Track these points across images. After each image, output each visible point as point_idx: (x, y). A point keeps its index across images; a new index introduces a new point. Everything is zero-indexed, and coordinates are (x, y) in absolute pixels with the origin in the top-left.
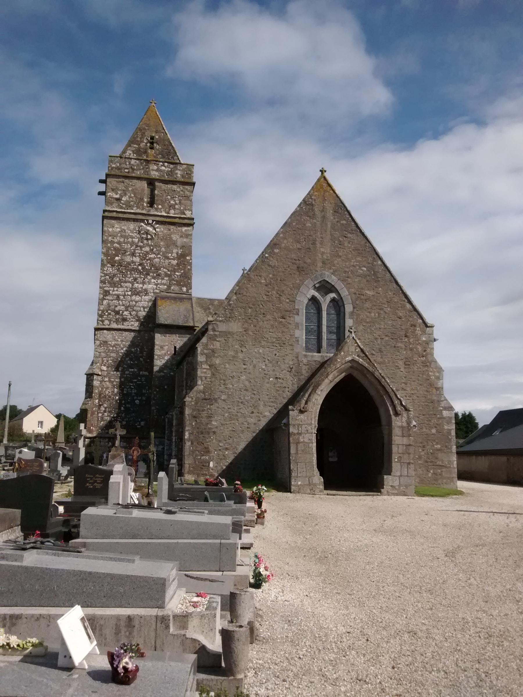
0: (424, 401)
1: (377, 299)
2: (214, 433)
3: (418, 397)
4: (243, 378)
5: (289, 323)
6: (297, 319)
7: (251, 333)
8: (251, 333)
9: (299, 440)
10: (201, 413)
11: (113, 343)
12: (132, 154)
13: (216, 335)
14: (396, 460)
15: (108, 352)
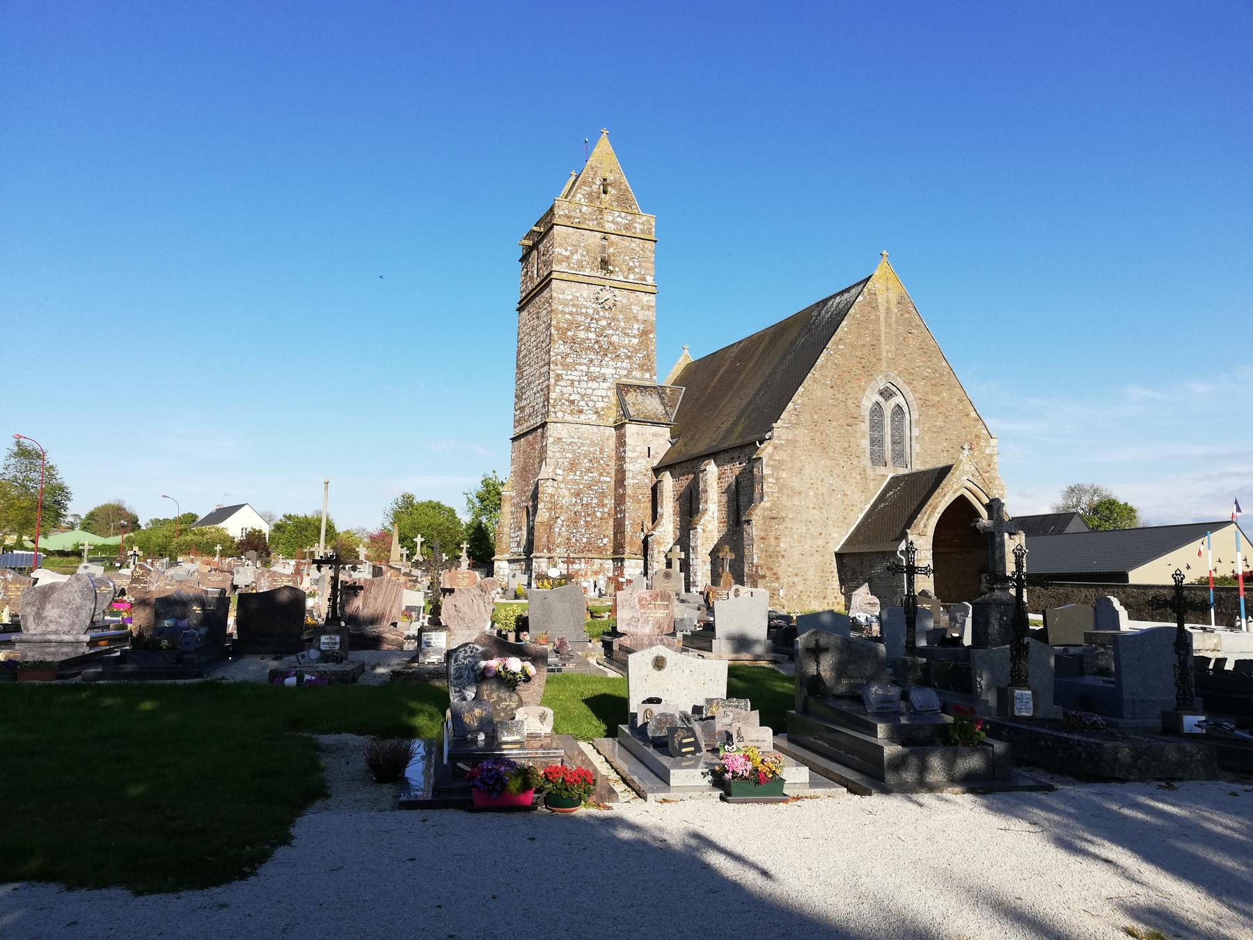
2: (783, 556)
8: (818, 442)
13: (782, 445)
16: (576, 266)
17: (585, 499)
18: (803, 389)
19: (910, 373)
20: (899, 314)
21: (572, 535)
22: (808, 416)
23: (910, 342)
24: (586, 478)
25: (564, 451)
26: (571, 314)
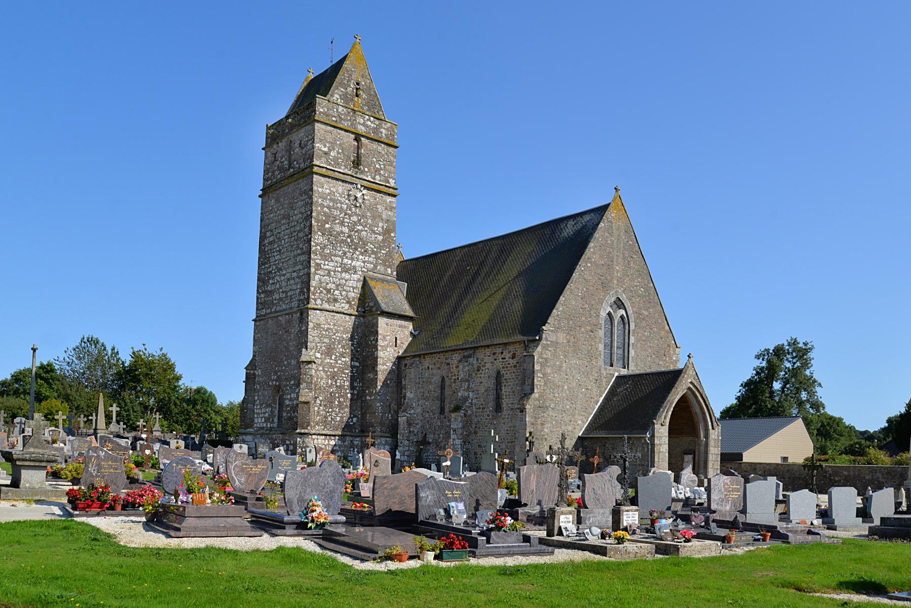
2: (546, 439)
17: (338, 381)
18: (564, 299)
19: (631, 291)
24: (339, 362)
26: (328, 207)
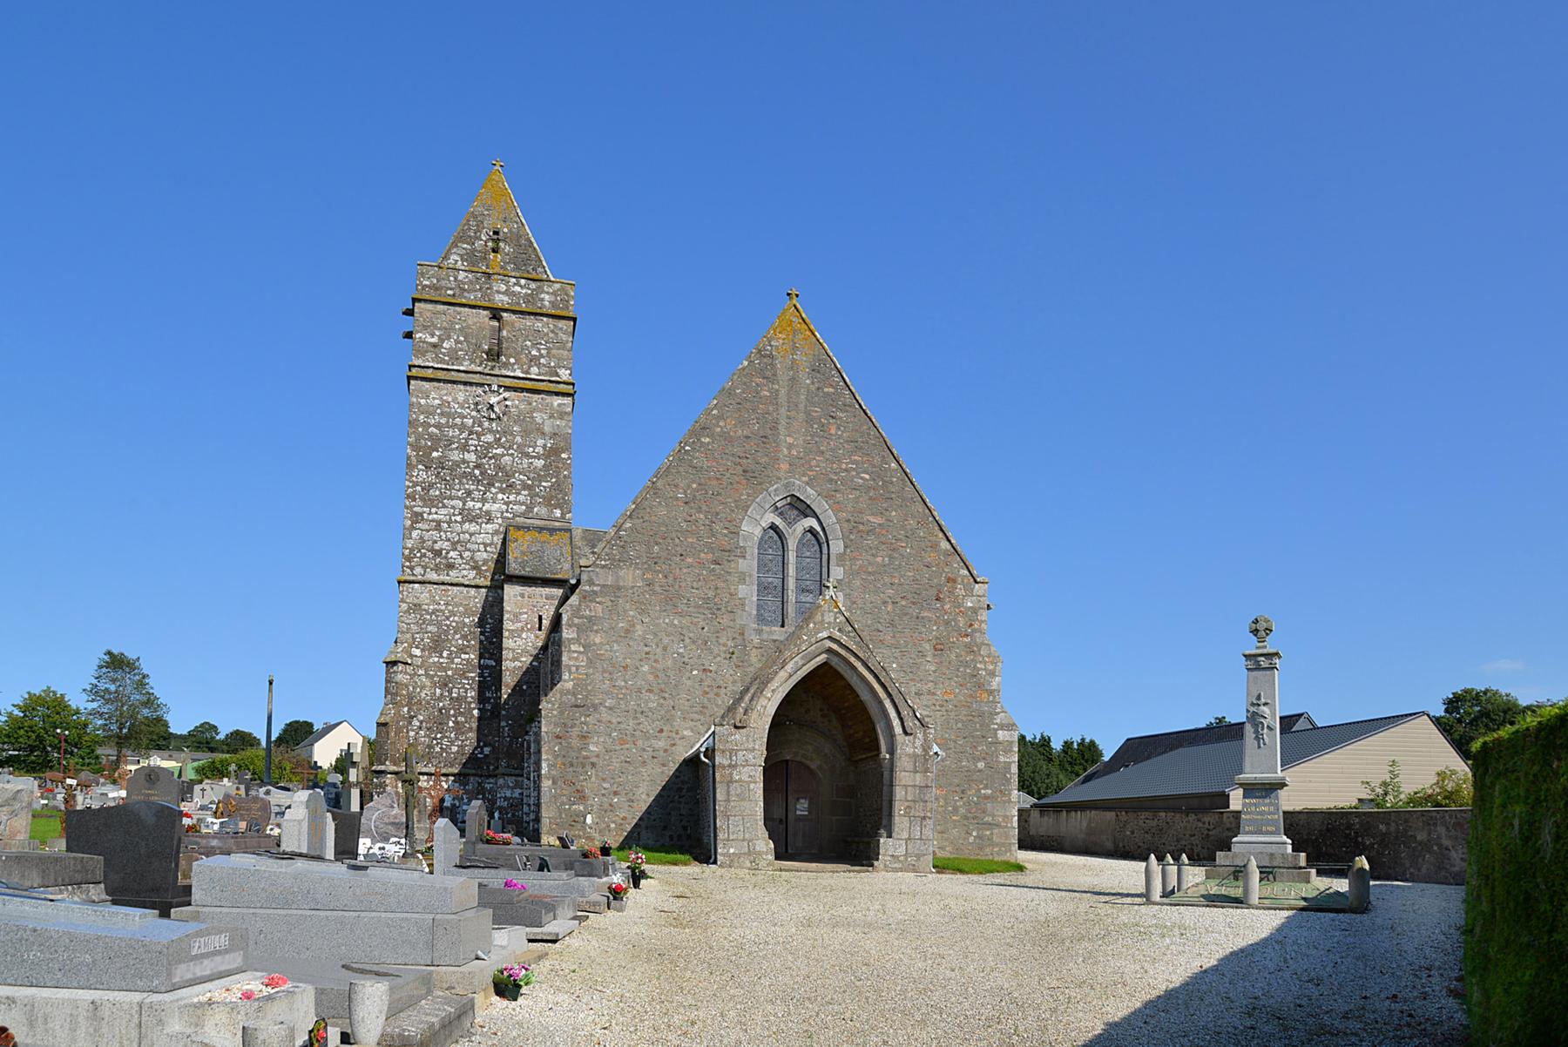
0: (965, 713)
1: (887, 531)
2: (593, 765)
3: (956, 706)
4: (646, 668)
5: (728, 572)
6: (742, 565)
7: (658, 589)
8: (658, 589)
9: (732, 778)
10: (569, 730)
11: (431, 607)
12: (460, 262)
13: (595, 593)
14: (902, 812)
15: (424, 623)
16: (446, 358)
19: (831, 480)
20: (813, 388)
21: (435, 742)
22: (641, 548)
23: (833, 432)
24: (456, 660)
25: (424, 623)
26: (438, 426)
